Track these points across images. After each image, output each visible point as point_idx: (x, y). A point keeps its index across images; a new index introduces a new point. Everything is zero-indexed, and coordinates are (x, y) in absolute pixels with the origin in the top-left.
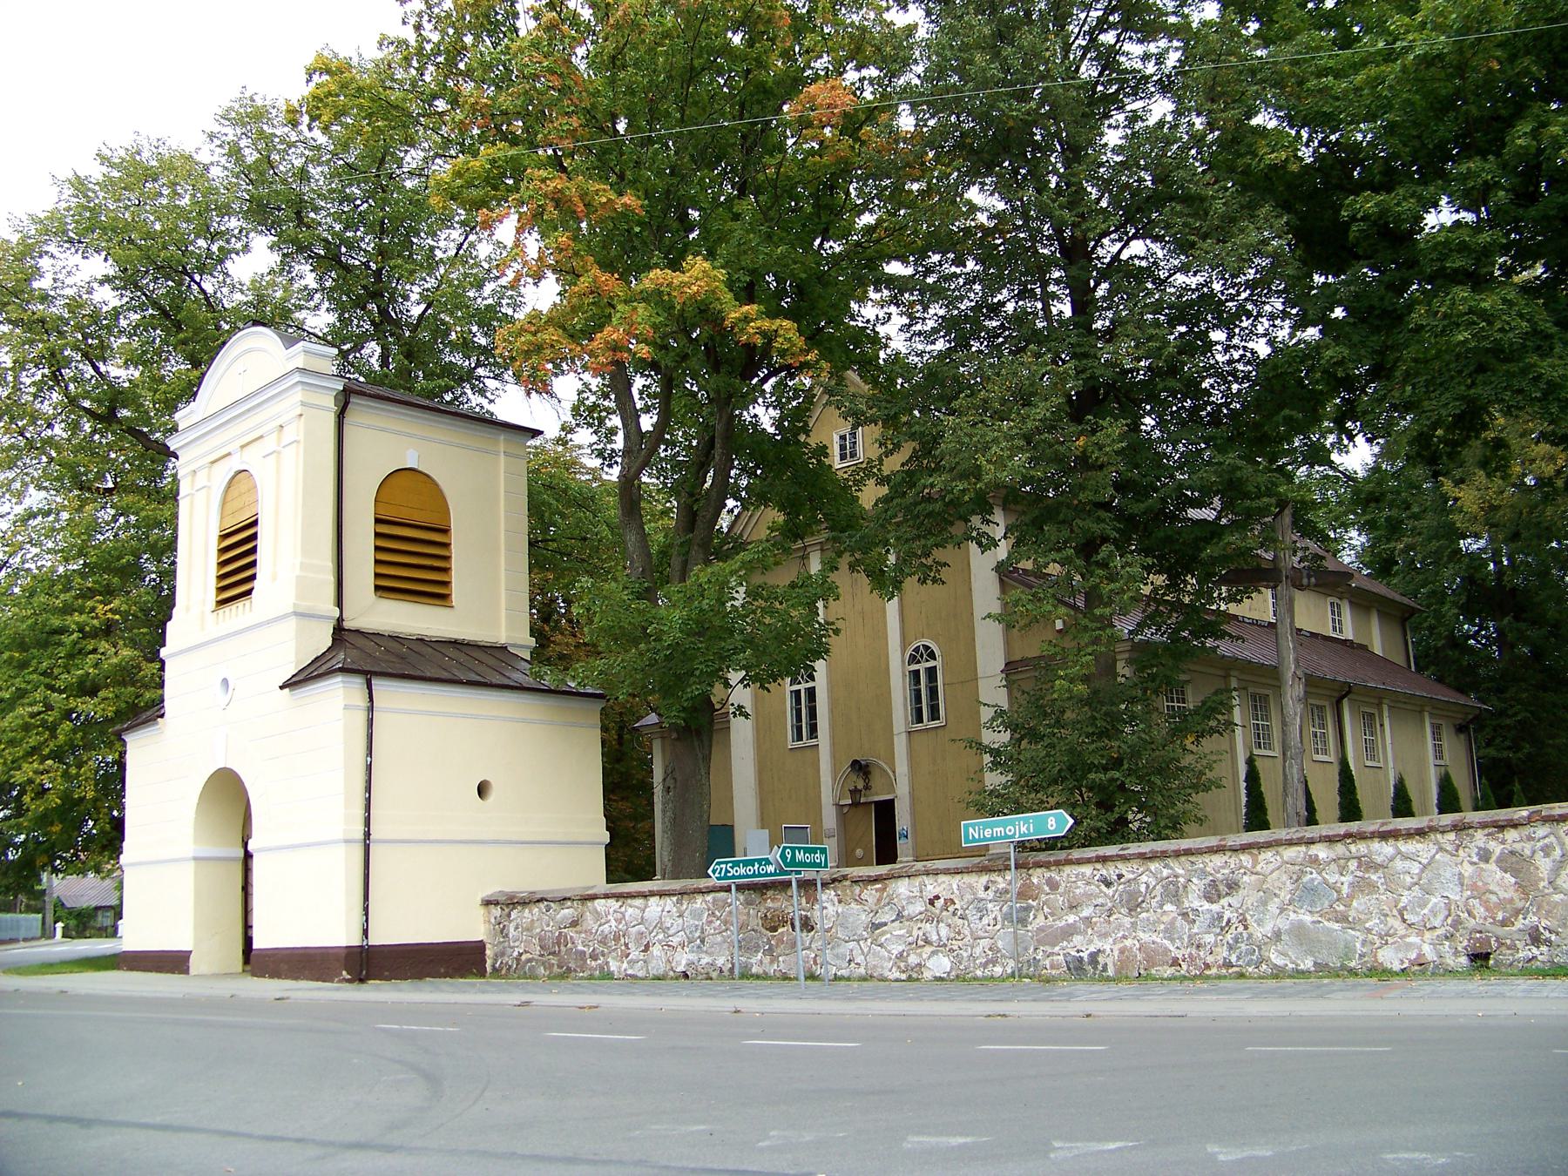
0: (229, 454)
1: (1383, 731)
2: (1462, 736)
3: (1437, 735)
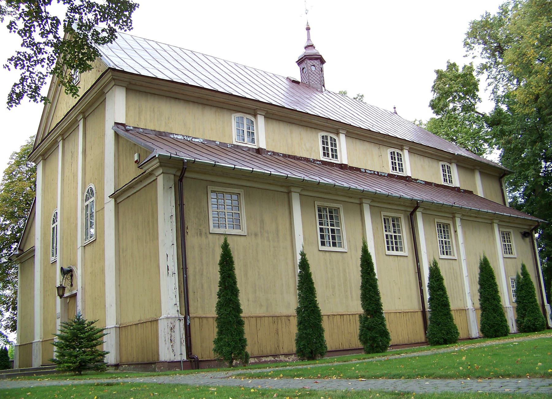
0: (227, 262)
1: (456, 236)
2: (528, 240)
3: (505, 237)
